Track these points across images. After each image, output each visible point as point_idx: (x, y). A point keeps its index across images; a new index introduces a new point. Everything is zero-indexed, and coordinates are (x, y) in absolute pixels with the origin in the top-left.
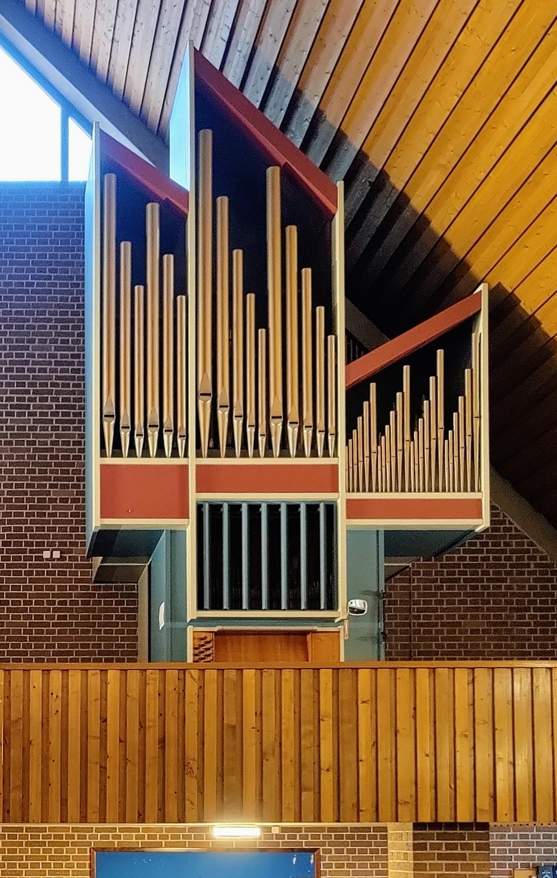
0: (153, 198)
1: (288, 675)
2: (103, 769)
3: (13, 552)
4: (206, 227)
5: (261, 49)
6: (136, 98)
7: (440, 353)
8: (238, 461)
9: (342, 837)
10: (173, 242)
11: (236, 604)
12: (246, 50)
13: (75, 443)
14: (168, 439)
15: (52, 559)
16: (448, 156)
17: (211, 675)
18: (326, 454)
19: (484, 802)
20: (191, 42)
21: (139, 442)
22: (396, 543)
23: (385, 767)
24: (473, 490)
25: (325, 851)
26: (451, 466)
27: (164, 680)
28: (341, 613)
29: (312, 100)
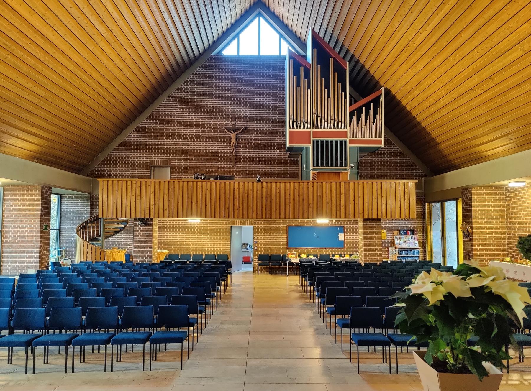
1: (333, 184)
2: (289, 206)
4: (315, 72)
5: (329, 28)
10: (307, 76)
11: (322, 165)
12: (325, 29)
14: (306, 125)
17: (315, 184)
18: (344, 129)
19: (379, 214)
21: (298, 125)
22: (361, 150)
23: (356, 205)
26: (375, 132)
27: (304, 185)
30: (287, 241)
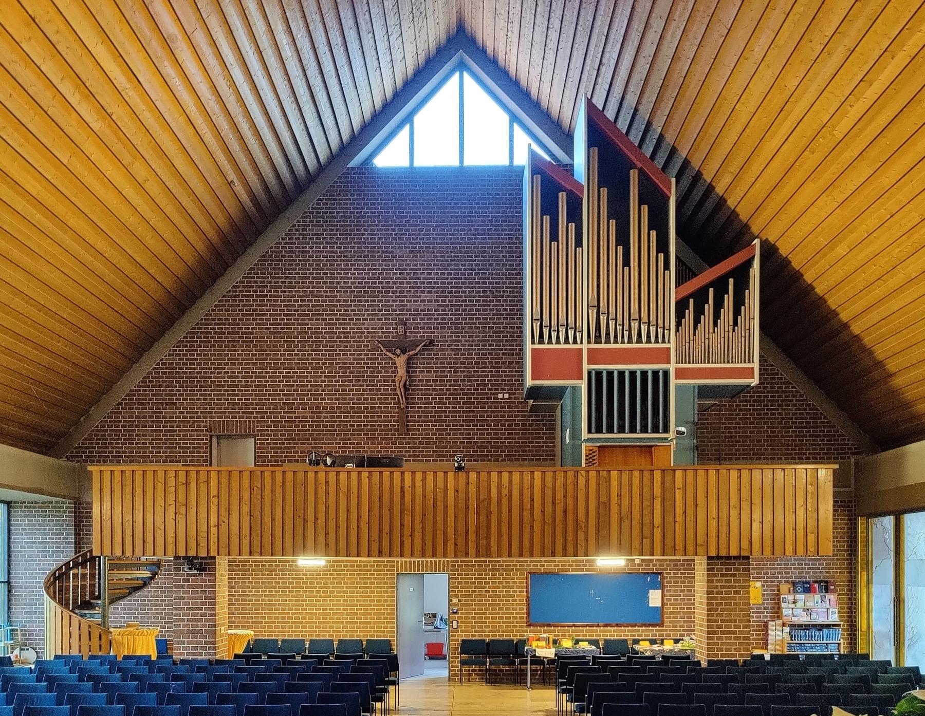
0: (562, 189)
2: (532, 527)
3: (481, 394)
5: (627, 97)
6: (555, 112)
7: (731, 281)
8: (612, 346)
9: (677, 565)
10: (574, 214)
11: (610, 430)
12: (619, 97)
13: (517, 328)
14: (571, 333)
15: (503, 398)
16: (734, 167)
17: (593, 474)
18: (664, 342)
19: (745, 544)
20: (586, 94)
21: (554, 335)
23: (690, 525)
24: (749, 362)
25: (667, 574)
27: (566, 477)
28: (671, 435)
29: (657, 128)
30: (528, 609)
